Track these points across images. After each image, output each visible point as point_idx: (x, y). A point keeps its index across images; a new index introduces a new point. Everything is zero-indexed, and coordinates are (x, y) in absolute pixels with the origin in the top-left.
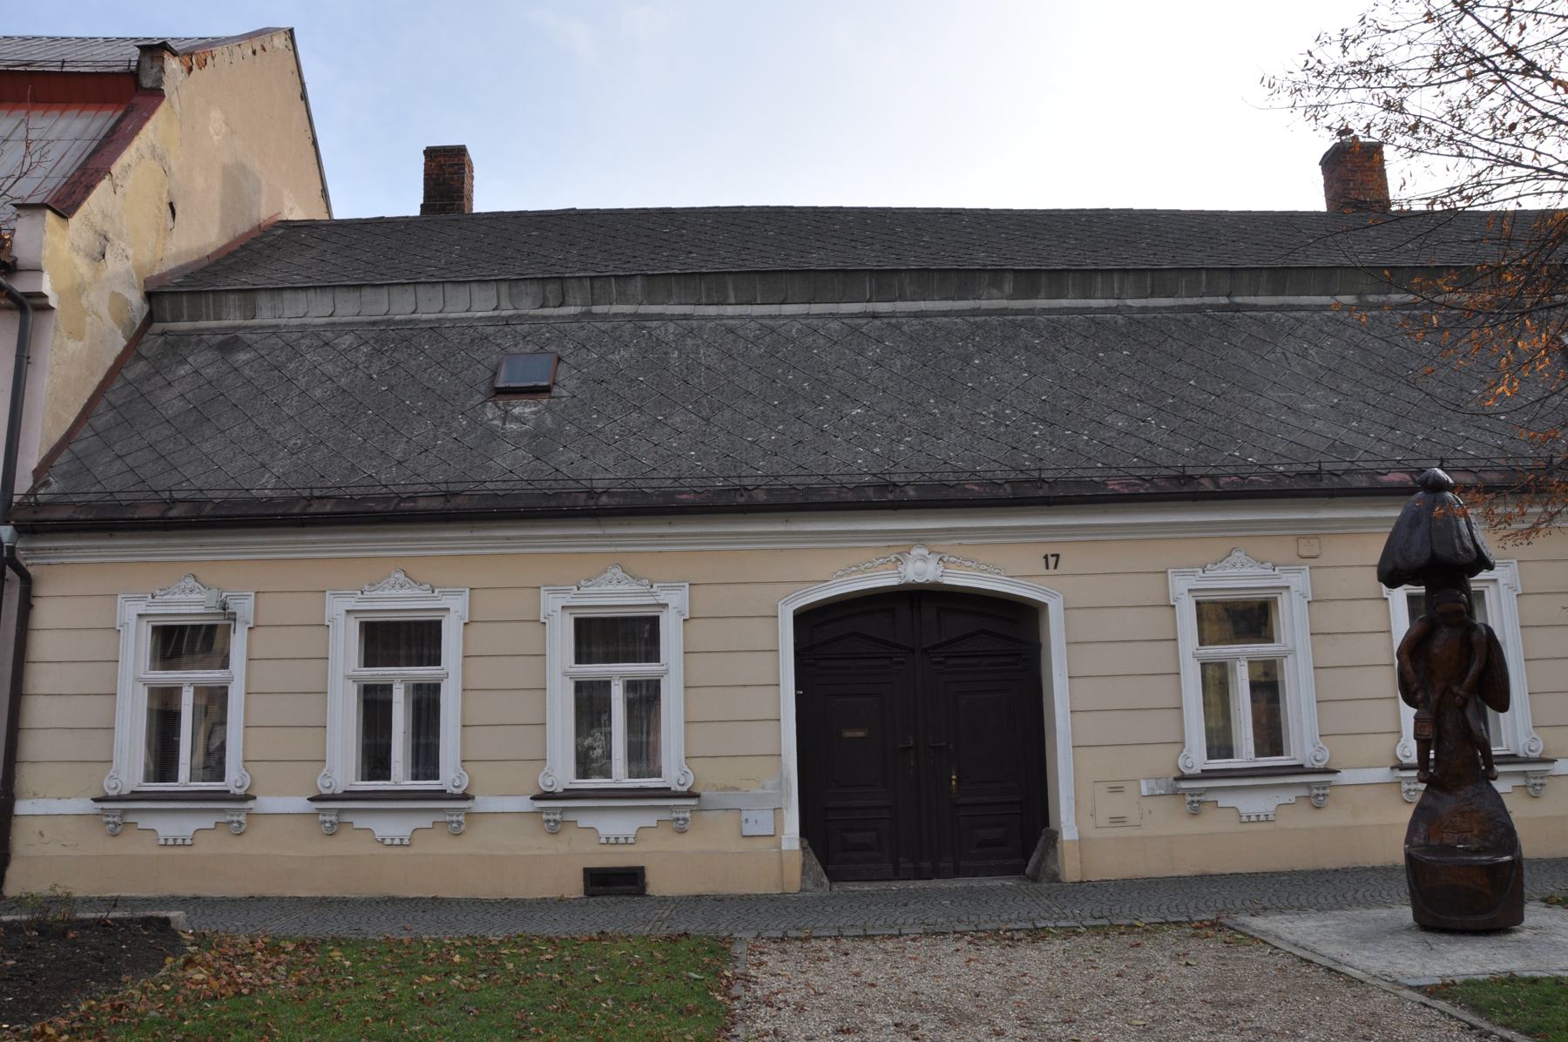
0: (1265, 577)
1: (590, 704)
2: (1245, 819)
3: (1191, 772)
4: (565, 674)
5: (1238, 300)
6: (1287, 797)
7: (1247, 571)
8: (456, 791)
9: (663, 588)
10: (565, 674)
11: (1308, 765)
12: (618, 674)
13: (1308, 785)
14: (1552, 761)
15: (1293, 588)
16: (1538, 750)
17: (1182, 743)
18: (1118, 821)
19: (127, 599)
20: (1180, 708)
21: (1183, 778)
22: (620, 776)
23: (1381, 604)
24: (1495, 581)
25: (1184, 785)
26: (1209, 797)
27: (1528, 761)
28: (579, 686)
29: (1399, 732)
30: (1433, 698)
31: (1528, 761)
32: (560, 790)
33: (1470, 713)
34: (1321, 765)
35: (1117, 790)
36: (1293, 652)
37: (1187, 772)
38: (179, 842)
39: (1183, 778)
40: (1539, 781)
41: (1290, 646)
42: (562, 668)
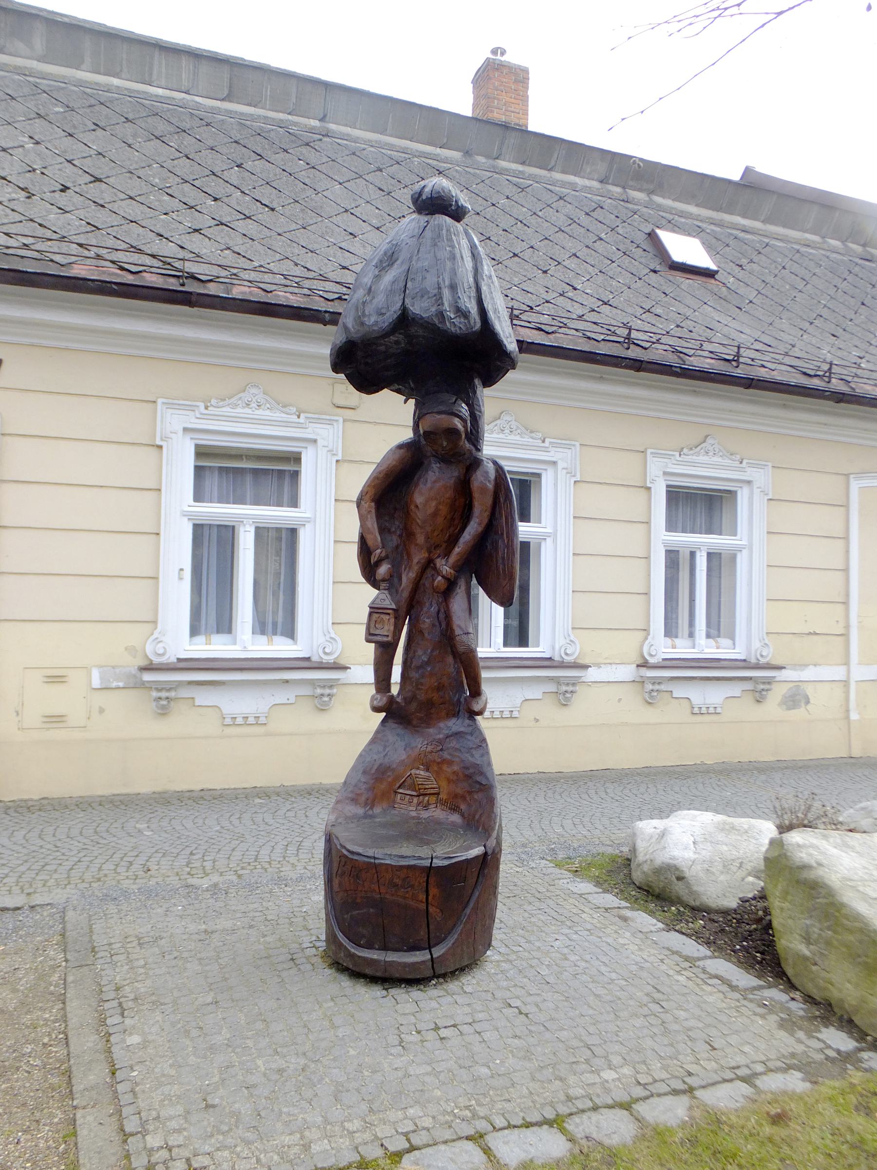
0: (286, 424)
1: (213, 546)
2: (228, 721)
3: (163, 660)
4: (184, 514)
5: (658, 199)
6: (282, 696)
7: (514, 438)
8: (326, 659)
9: (311, 420)
10: (184, 514)
11: (315, 658)
12: (248, 516)
13: (312, 683)
14: (585, 667)
15: (320, 442)
16: (573, 654)
17: (155, 622)
18: (56, 720)
19: (170, 406)
20: (156, 578)
21: (150, 668)
22: (245, 642)
23: (153, 451)
24: (554, 463)
25: (148, 677)
26: (184, 693)
27: (562, 665)
28: (199, 531)
29: (646, 630)
30: (407, 578)
31: (562, 665)
32: (173, 660)
33: (457, 604)
34: (330, 659)
35: (56, 679)
36: (554, 535)
37: (156, 660)
38: (506, 714)
39: (150, 668)
40: (570, 688)
41: (549, 530)
42: (181, 506)
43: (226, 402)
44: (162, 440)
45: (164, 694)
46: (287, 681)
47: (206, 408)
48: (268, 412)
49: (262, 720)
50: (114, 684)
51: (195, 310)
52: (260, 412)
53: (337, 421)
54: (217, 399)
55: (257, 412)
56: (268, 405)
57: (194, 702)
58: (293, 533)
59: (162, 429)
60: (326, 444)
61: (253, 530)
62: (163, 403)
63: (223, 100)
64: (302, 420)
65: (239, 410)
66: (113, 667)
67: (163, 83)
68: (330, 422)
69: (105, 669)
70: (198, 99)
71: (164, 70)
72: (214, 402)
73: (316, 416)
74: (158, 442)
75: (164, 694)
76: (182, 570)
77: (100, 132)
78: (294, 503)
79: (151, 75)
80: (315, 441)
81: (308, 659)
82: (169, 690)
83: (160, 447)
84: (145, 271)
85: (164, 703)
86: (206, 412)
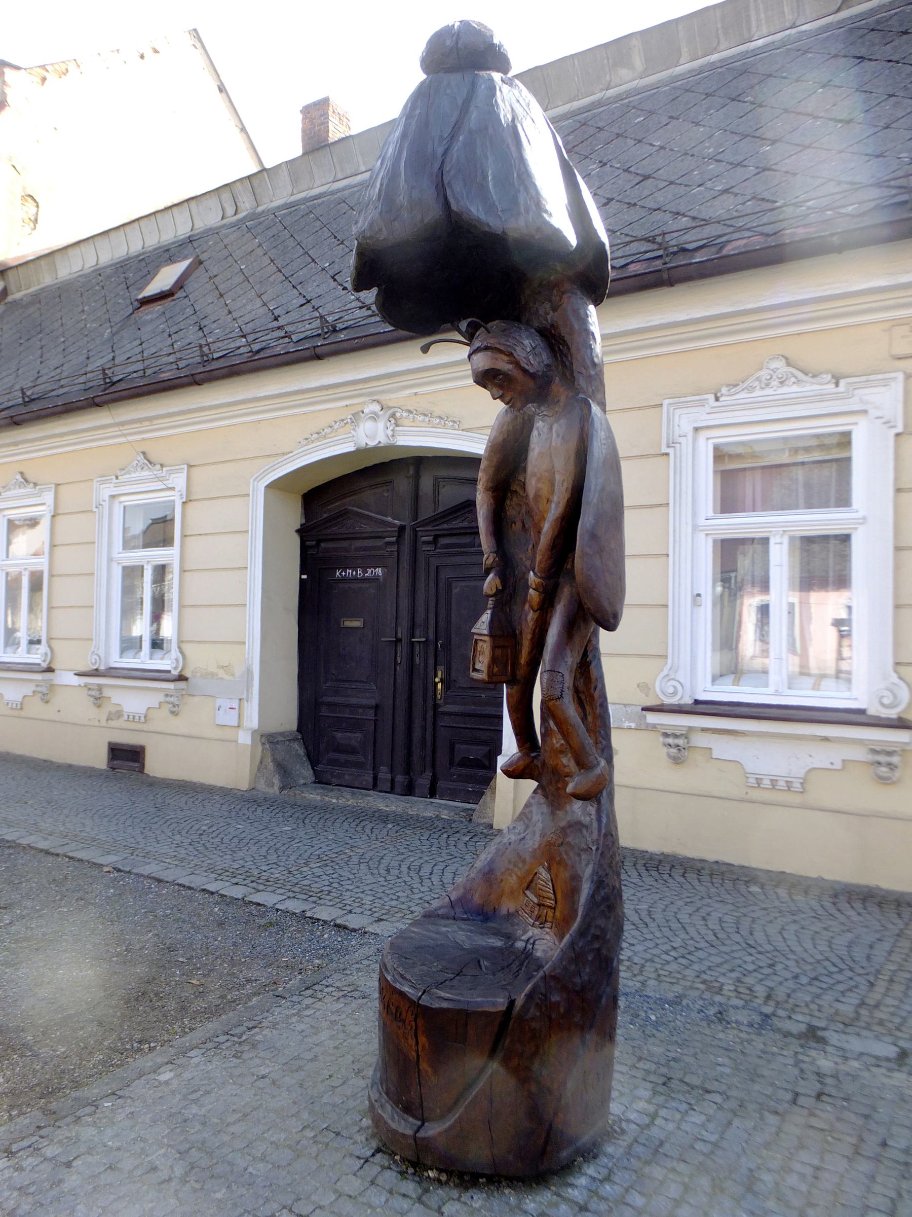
0: (821, 398)
11: (872, 711)
43: (739, 388)
44: (668, 446)
45: (883, 759)
46: (826, 739)
47: (717, 399)
48: (795, 388)
49: (797, 786)
50: (626, 724)
51: (680, 288)
52: (785, 390)
53: (895, 378)
54: (728, 385)
55: (781, 391)
56: (793, 380)
57: (711, 754)
58: (845, 539)
59: (668, 434)
60: (879, 414)
61: (786, 540)
62: (670, 404)
63: (838, 10)
64: (841, 388)
65: (758, 393)
66: (625, 705)
67: (765, 31)
68: (885, 383)
69: (617, 706)
70: (804, 28)
71: (762, 16)
72: (724, 390)
73: (864, 378)
74: (664, 450)
75: (883, 759)
76: (699, 595)
77: (674, 122)
78: (843, 500)
79: (749, 30)
80: (865, 412)
81: (862, 712)
82: (890, 753)
83: (667, 454)
84: (632, 262)
85: (884, 770)
86: (717, 404)
